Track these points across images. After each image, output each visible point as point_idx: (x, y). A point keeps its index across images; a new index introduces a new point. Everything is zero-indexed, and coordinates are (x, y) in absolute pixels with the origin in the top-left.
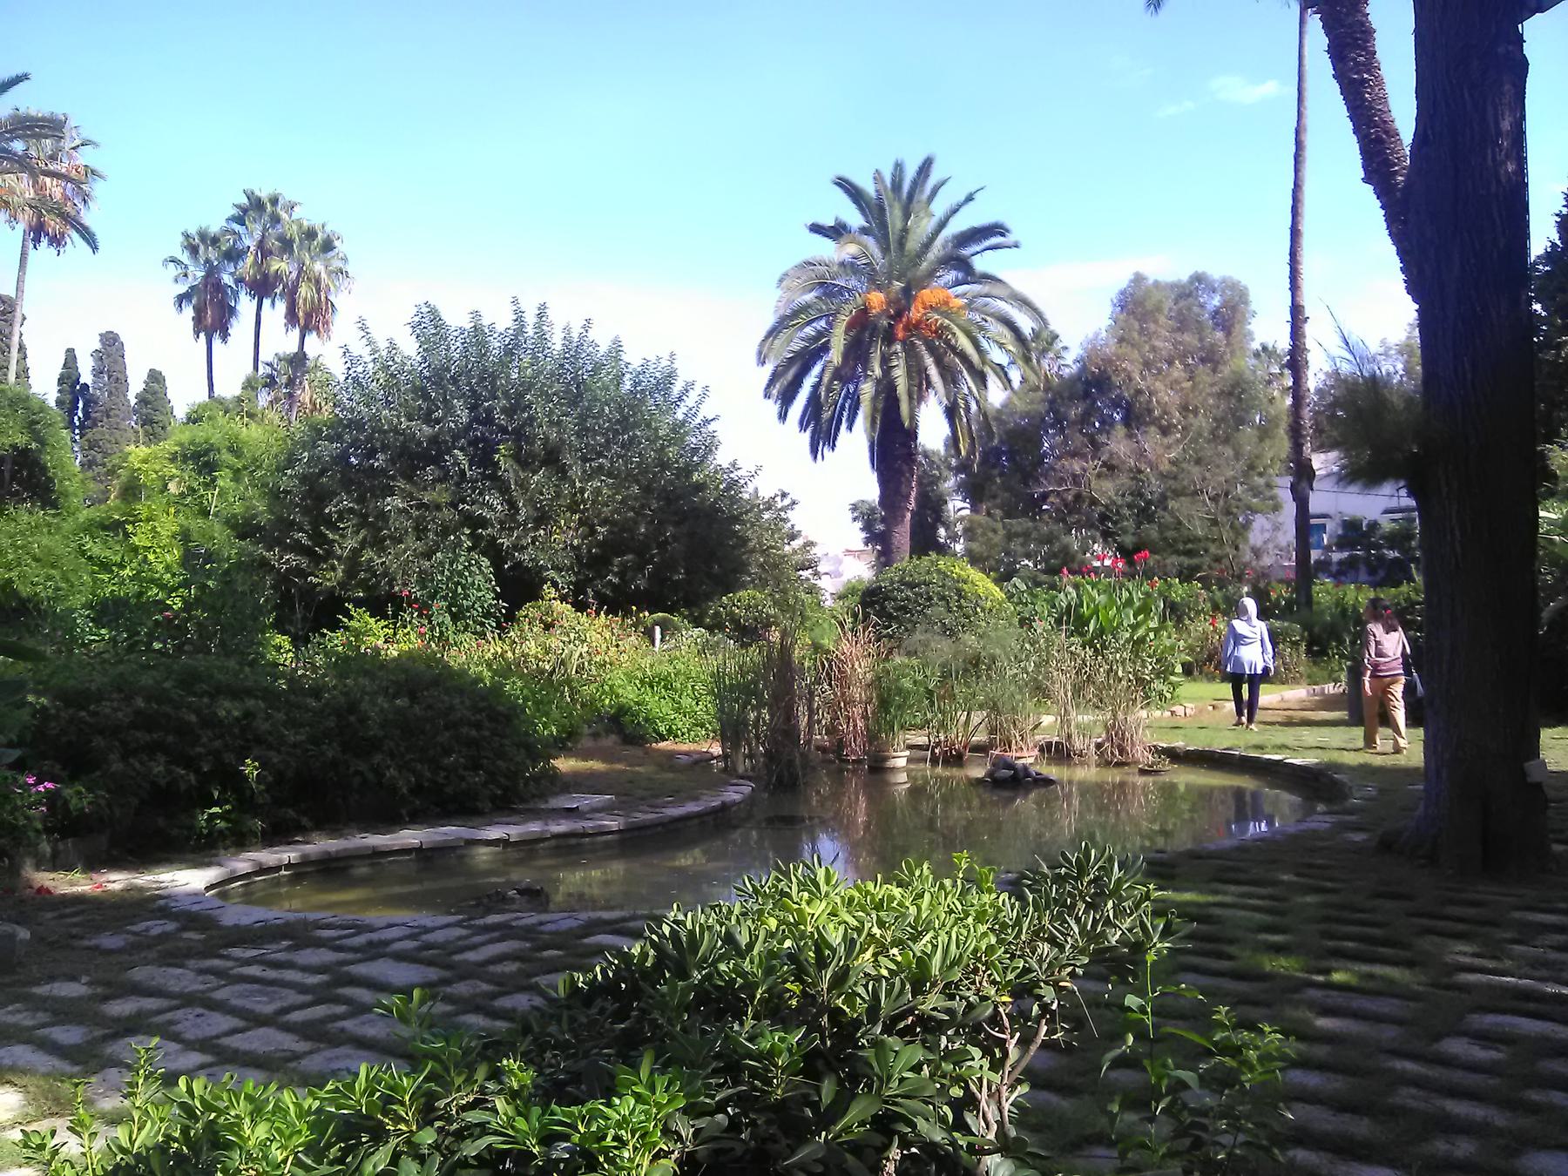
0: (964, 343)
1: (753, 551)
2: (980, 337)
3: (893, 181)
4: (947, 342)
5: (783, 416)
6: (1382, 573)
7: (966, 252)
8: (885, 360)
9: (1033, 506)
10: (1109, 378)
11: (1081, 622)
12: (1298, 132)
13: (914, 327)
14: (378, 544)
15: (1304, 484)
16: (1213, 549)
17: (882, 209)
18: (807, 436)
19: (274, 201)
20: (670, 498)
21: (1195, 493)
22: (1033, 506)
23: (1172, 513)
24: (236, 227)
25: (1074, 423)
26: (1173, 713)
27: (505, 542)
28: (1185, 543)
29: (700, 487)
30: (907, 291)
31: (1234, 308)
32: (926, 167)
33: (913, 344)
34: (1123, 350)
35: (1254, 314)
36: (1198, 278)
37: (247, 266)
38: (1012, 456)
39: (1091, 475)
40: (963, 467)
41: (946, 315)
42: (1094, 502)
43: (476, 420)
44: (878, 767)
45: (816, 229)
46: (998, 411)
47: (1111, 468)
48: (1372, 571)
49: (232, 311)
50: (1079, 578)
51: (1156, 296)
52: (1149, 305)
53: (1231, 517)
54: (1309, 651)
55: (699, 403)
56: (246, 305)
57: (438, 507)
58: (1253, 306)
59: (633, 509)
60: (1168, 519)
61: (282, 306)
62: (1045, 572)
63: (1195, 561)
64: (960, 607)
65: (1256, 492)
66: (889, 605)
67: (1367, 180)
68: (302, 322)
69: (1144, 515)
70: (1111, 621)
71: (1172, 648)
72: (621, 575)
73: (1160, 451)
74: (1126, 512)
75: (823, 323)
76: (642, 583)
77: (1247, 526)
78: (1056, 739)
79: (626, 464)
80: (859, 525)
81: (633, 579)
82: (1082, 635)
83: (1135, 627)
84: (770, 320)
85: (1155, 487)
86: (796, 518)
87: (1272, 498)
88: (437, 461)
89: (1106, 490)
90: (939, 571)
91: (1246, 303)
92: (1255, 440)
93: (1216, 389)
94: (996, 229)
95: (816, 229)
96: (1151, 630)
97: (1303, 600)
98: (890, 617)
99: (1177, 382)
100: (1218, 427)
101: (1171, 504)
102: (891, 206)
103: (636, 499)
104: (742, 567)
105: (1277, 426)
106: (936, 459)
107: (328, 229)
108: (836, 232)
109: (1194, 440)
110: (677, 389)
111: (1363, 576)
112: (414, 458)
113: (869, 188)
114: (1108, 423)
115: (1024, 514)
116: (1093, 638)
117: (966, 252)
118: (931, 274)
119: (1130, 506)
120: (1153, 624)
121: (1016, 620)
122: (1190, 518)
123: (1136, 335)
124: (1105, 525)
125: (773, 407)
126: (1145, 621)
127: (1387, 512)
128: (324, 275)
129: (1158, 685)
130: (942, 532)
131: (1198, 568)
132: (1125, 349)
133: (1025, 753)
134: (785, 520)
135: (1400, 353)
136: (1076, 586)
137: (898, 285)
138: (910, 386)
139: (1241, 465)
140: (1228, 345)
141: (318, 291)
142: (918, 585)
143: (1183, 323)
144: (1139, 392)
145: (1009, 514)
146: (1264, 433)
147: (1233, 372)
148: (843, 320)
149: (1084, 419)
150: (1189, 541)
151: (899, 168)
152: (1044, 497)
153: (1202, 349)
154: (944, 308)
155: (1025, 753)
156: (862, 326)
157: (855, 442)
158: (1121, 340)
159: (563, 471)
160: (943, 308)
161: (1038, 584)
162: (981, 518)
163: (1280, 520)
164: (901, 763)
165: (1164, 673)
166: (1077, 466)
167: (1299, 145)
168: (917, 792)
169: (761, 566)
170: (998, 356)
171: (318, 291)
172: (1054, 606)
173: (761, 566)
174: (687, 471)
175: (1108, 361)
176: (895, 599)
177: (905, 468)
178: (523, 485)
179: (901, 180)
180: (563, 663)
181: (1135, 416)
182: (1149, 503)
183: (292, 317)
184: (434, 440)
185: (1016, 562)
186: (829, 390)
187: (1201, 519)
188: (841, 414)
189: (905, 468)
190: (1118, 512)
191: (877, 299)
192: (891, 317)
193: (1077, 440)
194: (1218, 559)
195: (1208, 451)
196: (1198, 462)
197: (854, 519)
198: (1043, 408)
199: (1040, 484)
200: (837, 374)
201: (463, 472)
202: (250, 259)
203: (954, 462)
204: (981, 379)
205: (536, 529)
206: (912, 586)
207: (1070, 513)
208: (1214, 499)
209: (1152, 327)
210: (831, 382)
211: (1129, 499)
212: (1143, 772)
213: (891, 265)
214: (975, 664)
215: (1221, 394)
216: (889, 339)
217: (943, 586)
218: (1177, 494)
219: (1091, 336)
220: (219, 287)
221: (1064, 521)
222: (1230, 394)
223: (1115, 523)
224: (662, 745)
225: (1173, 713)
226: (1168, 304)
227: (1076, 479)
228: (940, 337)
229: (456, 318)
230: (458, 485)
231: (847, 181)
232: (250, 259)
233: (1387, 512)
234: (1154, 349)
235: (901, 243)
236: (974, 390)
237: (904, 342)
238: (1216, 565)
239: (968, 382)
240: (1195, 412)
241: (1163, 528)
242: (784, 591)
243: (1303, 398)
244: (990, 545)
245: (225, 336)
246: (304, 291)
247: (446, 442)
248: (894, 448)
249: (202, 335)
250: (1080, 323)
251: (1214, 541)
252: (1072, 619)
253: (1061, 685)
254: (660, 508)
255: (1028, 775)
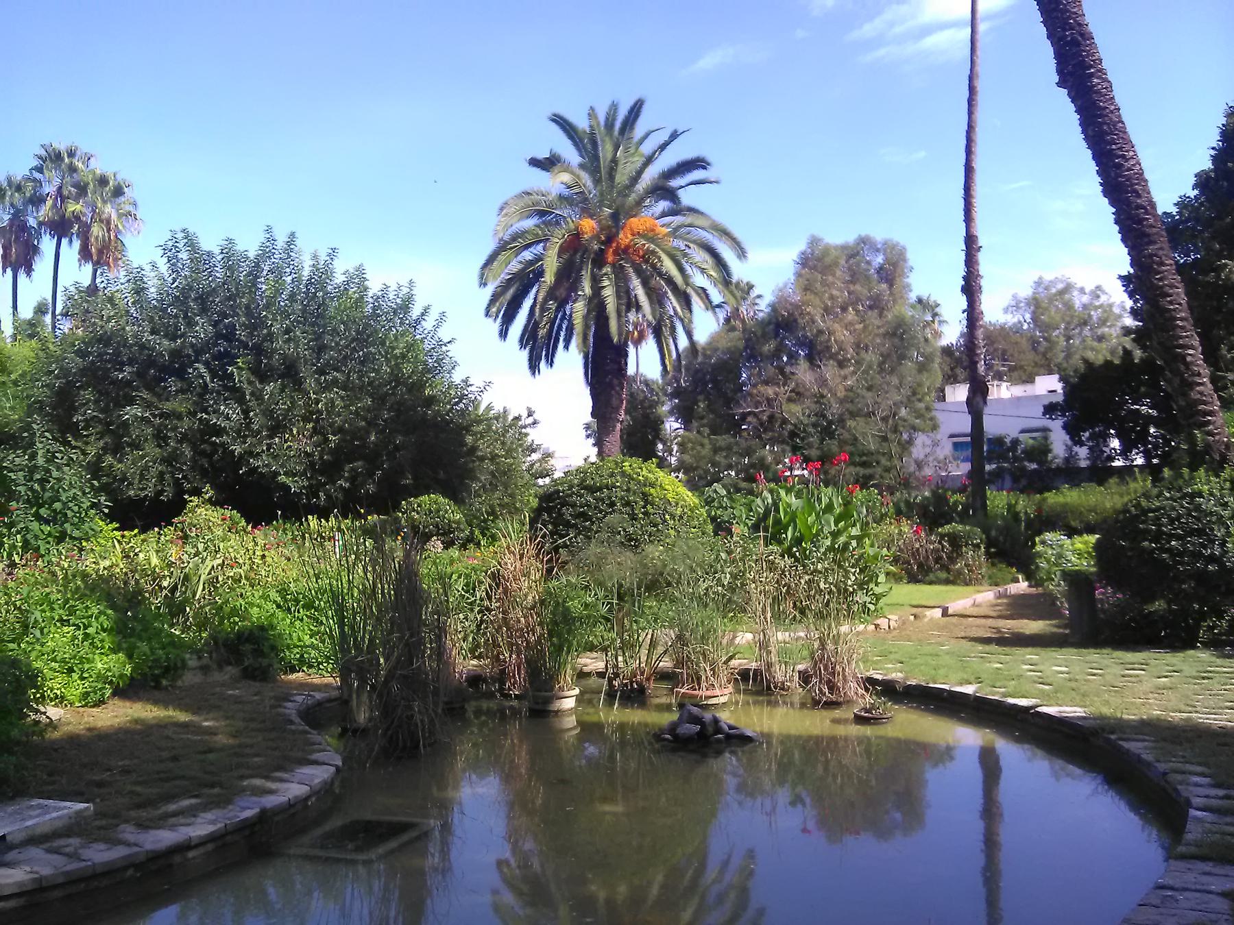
0: (668, 266)
1: (482, 459)
2: (683, 262)
3: (607, 119)
4: (654, 266)
5: (503, 334)
6: (1024, 482)
7: (674, 183)
8: (596, 281)
9: (734, 427)
10: (795, 321)
11: (780, 527)
12: (971, 79)
13: (624, 252)
14: (116, 449)
15: (979, 399)
16: (884, 461)
17: (594, 143)
18: (525, 354)
19: (71, 154)
20: (400, 408)
21: (868, 415)
22: (734, 427)
23: (849, 431)
24: (37, 175)
25: (768, 357)
26: (877, 626)
27: (237, 449)
28: (860, 456)
29: (431, 401)
30: (615, 217)
31: (895, 265)
32: (636, 110)
33: (622, 267)
34: (808, 297)
35: (911, 269)
36: (864, 241)
37: (45, 211)
38: (715, 381)
39: (783, 399)
40: (677, 393)
41: (652, 240)
42: (785, 421)
43: (219, 335)
44: (540, 708)
45: (534, 162)
46: (703, 349)
47: (798, 395)
48: (1015, 480)
49: (36, 250)
50: (772, 485)
51: (834, 253)
52: (828, 260)
53: (897, 433)
54: (987, 553)
55: (436, 327)
56: (47, 244)
57: (179, 417)
58: (911, 263)
59: (364, 419)
60: (846, 436)
61: (77, 244)
62: (744, 480)
63: (868, 471)
64: (646, 514)
65: (919, 416)
66: (567, 512)
67: (1059, 84)
68: (95, 258)
69: (827, 432)
70: (810, 528)
71: (875, 557)
72: (352, 479)
73: (838, 380)
74: (811, 430)
75: (540, 247)
76: (371, 488)
77: (910, 442)
78: (754, 665)
79: (360, 378)
80: (591, 441)
81: (363, 484)
82: (780, 542)
83: (835, 535)
84: (490, 246)
85: (835, 409)
86: (534, 436)
87: (932, 419)
88: (181, 374)
89: (796, 412)
90: (623, 474)
91: (905, 260)
92: (914, 372)
93: (882, 331)
94: (698, 163)
95: (534, 162)
96: (853, 538)
97: (978, 504)
98: (568, 525)
99: (851, 324)
100: (884, 362)
101: (850, 423)
102: (603, 141)
103: (369, 411)
104: (470, 474)
105: (933, 361)
106: (655, 387)
107: (119, 177)
108: (548, 164)
109: (866, 372)
110: (416, 312)
111: (1008, 482)
112: (157, 372)
113: (582, 123)
114: (793, 357)
115: (727, 432)
116: (790, 548)
117: (674, 183)
118: (639, 203)
119: (815, 425)
120: (855, 531)
121: (710, 528)
122: (864, 435)
123: (818, 285)
124: (794, 440)
125: (494, 326)
126: (846, 529)
127: (1023, 431)
128: (114, 216)
129: (861, 597)
130: (660, 446)
131: (871, 477)
132: (810, 296)
133: (717, 692)
134: (526, 435)
135: (1028, 304)
136: (771, 491)
137: (607, 211)
138: (619, 305)
139: (906, 391)
140: (891, 294)
141: (109, 230)
142: (600, 489)
143: (855, 276)
144: (820, 332)
145: (714, 432)
146: (922, 368)
147: (897, 317)
148: (556, 242)
149: (776, 354)
150: (864, 454)
151: (614, 107)
152: (744, 417)
153: (869, 298)
154: (651, 234)
155: (717, 692)
156: (574, 246)
157: (570, 362)
158: (806, 289)
159: (298, 383)
160: (650, 235)
161: (738, 490)
162: (693, 435)
163: (939, 437)
164: (569, 703)
165: (867, 578)
166: (770, 391)
167: (972, 90)
168: (590, 730)
169: (492, 474)
170: (699, 280)
171: (109, 230)
172: (751, 510)
173: (492, 474)
174: (420, 385)
175: (796, 306)
176: (574, 505)
177: (615, 382)
178: (257, 395)
179: (614, 120)
180: (187, 578)
181: (816, 352)
182: (830, 423)
183: (85, 254)
184: (176, 354)
185: (719, 472)
186: (543, 310)
187: (873, 435)
188: (558, 334)
189: (615, 382)
190: (805, 431)
191: (589, 226)
192: (602, 243)
193: (771, 370)
194: (887, 470)
195: (878, 379)
196: (869, 389)
197: (588, 437)
198: (741, 344)
199: (740, 406)
200: (551, 294)
201: (206, 385)
202: (49, 203)
203: (669, 389)
204: (686, 302)
205: (271, 437)
206: (592, 490)
207: (765, 431)
208: (883, 419)
209: (830, 278)
210: (545, 301)
211: (813, 419)
212: (859, 720)
213: (602, 194)
214: (655, 584)
215: (886, 335)
216: (599, 261)
217: (628, 490)
218: (853, 415)
219: (781, 285)
220: (24, 227)
221: (760, 437)
222: (894, 334)
223: (802, 439)
224: (293, 677)
225: (877, 626)
226: (842, 262)
227: (770, 402)
228: (647, 261)
229: (210, 243)
230: (201, 396)
231: (565, 121)
232: (49, 203)
233: (1023, 431)
234: (832, 297)
235: (611, 177)
236: (679, 310)
237: (613, 265)
238: (886, 474)
239: (673, 303)
240: (866, 348)
241: (842, 443)
242: (512, 496)
243: (977, 320)
244: (699, 458)
245: (29, 271)
246: (96, 230)
247: (189, 356)
248: (605, 368)
249: (9, 271)
250: (768, 272)
251: (884, 454)
252: (769, 526)
253: (760, 586)
254: (391, 418)
255: (718, 730)
